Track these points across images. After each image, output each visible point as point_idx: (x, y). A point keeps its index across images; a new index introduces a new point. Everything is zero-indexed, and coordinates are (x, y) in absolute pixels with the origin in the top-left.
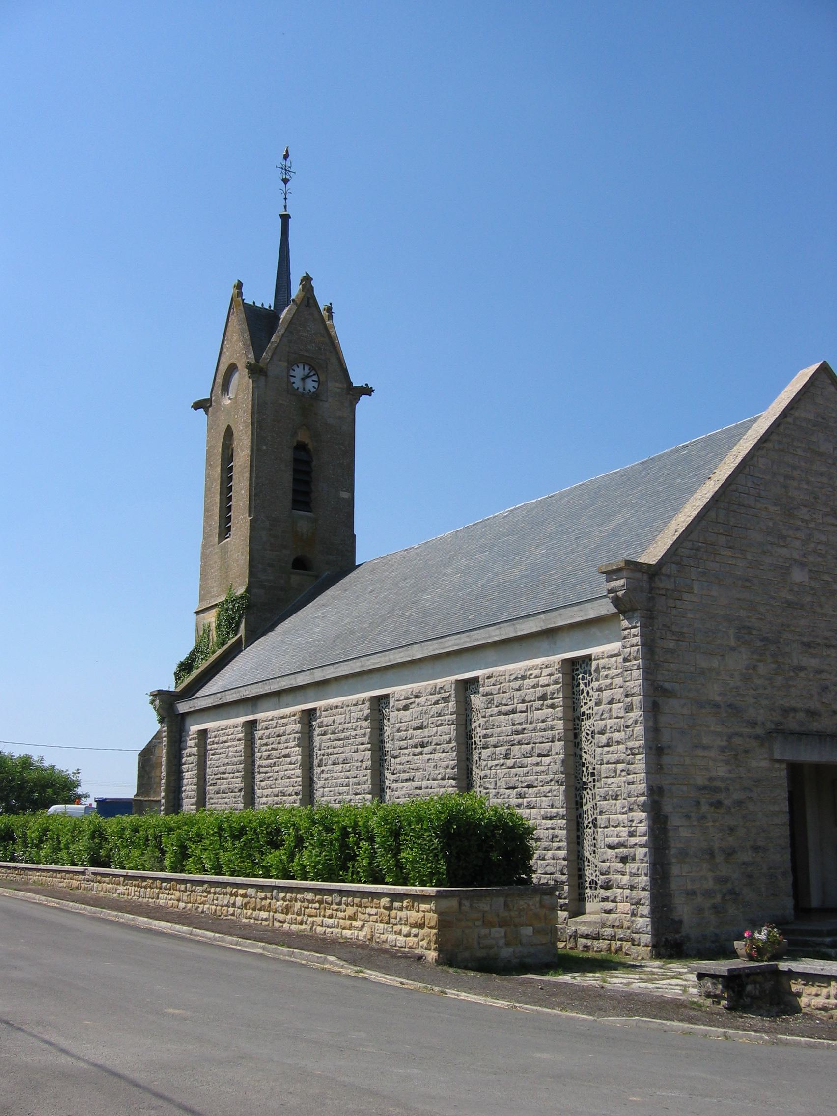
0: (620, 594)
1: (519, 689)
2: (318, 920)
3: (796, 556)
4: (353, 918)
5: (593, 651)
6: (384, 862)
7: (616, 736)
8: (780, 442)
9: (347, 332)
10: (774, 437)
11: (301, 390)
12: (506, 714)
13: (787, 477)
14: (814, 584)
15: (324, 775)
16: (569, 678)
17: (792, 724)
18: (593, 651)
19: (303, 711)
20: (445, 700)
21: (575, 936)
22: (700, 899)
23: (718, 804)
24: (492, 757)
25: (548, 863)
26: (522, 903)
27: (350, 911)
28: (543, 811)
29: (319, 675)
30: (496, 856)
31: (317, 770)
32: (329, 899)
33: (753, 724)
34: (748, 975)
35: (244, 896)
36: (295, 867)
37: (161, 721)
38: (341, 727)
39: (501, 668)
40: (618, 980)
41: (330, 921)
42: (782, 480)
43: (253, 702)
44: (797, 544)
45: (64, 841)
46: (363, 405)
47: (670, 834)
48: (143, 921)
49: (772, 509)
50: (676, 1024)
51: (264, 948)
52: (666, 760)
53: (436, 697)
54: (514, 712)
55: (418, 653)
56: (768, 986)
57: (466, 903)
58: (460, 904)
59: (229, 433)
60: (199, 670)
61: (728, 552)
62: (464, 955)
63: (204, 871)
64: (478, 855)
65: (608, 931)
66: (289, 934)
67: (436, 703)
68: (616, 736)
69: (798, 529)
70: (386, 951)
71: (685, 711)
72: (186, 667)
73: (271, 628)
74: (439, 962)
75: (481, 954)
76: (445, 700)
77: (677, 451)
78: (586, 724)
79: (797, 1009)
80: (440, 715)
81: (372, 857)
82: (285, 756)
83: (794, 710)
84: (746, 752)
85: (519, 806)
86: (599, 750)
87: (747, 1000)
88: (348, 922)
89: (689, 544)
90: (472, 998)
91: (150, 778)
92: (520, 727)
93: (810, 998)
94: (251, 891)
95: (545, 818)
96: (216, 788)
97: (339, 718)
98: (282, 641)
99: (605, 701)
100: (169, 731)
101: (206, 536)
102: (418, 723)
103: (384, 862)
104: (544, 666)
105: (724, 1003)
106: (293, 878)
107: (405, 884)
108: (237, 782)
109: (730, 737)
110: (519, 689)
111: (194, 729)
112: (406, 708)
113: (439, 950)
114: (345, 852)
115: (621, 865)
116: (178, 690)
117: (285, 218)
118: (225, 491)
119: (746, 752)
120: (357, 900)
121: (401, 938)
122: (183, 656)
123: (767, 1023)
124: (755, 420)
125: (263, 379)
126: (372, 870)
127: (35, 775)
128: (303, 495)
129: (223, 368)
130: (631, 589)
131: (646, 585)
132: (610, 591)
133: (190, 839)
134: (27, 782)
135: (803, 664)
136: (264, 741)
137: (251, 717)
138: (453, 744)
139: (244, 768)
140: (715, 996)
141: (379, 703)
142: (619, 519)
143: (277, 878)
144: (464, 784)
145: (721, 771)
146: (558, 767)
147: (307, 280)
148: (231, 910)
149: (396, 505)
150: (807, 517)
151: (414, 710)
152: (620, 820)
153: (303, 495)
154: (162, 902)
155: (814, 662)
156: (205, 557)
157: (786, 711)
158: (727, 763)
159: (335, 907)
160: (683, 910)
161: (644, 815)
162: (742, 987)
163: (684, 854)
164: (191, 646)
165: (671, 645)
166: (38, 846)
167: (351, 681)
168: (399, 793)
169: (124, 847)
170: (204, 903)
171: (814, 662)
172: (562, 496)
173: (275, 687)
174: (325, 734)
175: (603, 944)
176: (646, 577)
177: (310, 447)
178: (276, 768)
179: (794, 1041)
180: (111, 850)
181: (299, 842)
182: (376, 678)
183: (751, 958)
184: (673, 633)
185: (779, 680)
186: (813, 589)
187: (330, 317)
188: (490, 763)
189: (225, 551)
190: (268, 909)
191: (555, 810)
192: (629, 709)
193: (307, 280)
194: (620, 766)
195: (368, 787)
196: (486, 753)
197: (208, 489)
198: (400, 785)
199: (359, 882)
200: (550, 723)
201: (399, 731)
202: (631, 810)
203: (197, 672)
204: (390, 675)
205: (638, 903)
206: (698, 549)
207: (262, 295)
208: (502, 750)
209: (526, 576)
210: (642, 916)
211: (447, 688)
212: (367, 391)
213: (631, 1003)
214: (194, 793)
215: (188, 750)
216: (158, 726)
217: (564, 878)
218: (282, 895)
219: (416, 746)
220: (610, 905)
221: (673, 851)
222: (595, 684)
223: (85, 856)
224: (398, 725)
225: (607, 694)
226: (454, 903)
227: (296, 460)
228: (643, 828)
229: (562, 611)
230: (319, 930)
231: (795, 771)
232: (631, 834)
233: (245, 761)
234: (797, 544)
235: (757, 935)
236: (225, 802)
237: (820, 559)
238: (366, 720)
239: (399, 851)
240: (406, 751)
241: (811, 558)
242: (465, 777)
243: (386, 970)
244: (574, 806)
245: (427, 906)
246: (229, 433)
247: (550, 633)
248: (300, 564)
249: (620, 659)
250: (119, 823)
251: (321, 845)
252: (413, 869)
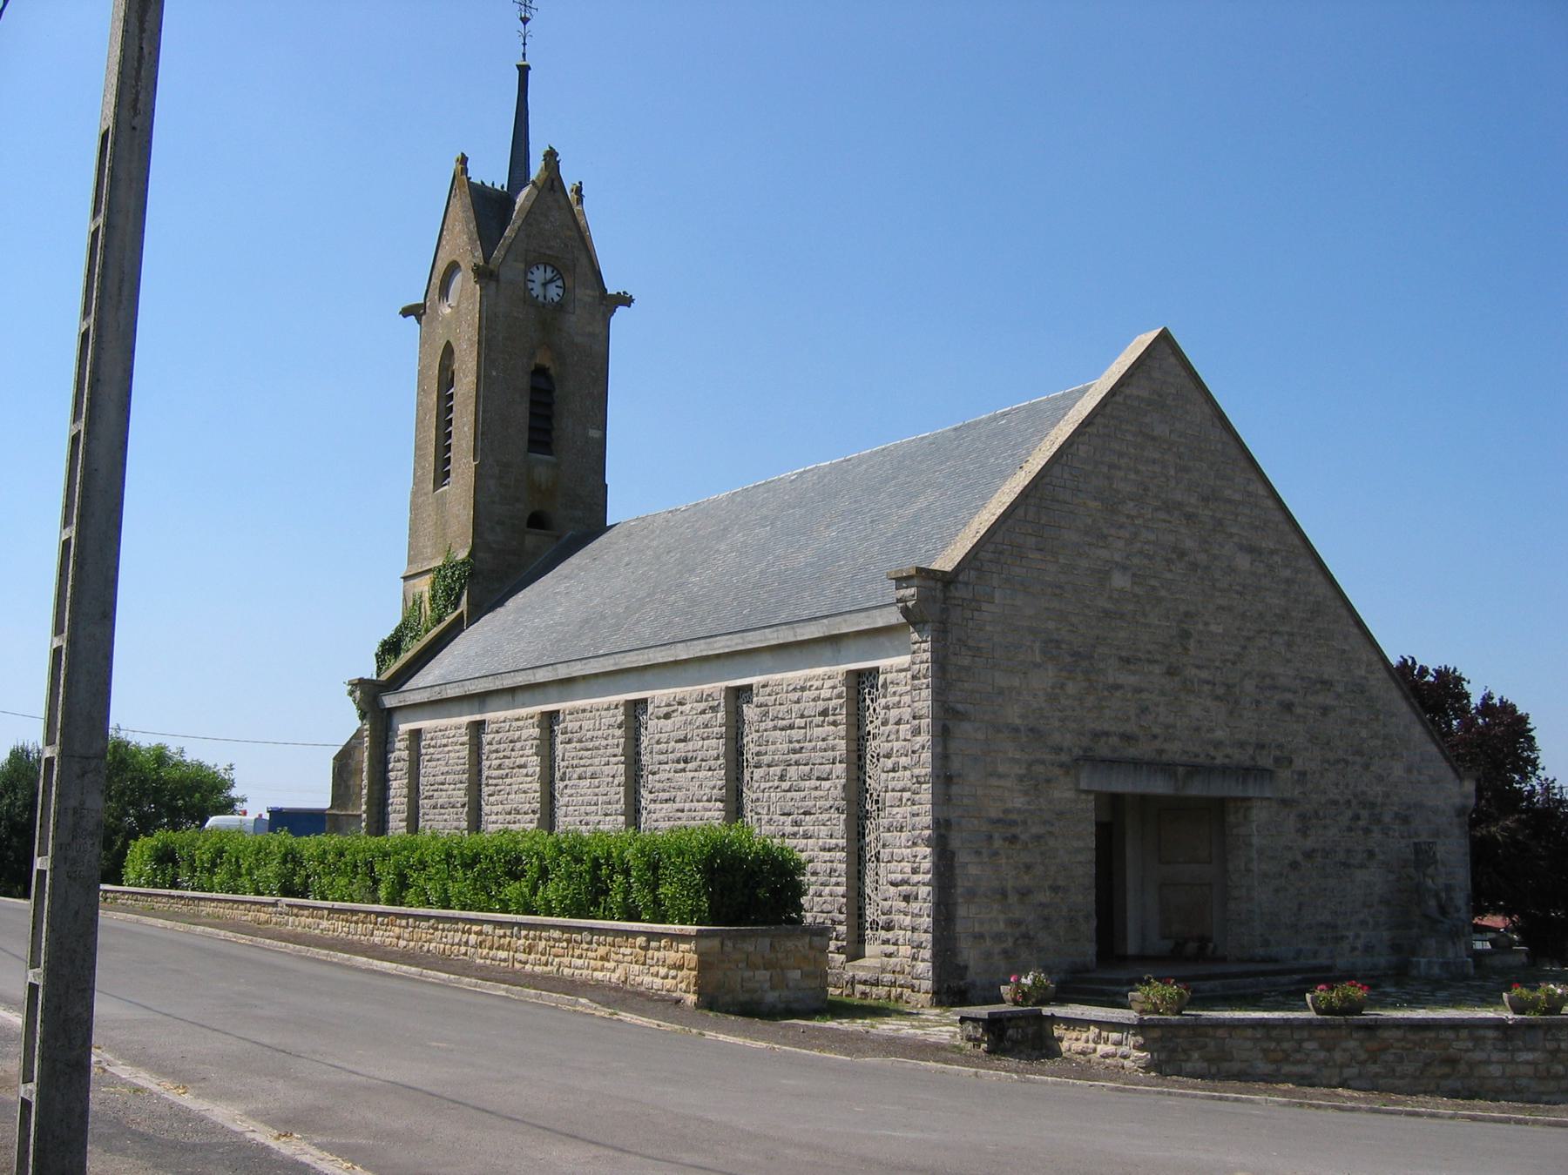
0: (910, 604)
1: (798, 702)
2: (566, 960)
3: (1117, 558)
4: (605, 958)
5: (882, 663)
6: (640, 897)
7: (903, 761)
8: (1105, 426)
9: (599, 219)
10: (1099, 420)
11: (541, 299)
12: (782, 729)
13: (1112, 466)
14: (1137, 590)
15: (568, 791)
16: (854, 692)
17: (1103, 750)
18: (882, 663)
19: (543, 713)
20: (714, 709)
21: (852, 982)
22: (989, 943)
23: (1013, 839)
24: (766, 778)
25: (822, 900)
26: (790, 944)
27: (602, 950)
28: (821, 842)
29: (563, 672)
30: (763, 893)
31: (559, 785)
32: (579, 938)
33: (1058, 750)
34: (1009, 1019)
35: (479, 933)
36: (538, 900)
37: (362, 717)
38: (589, 735)
39: (778, 676)
40: (887, 1027)
41: (580, 962)
42: (1105, 469)
43: (481, 699)
44: (1121, 544)
45: (245, 866)
46: (620, 319)
47: (958, 871)
48: (361, 960)
49: (1092, 504)
50: (931, 1064)
51: (507, 991)
52: (955, 790)
53: (703, 705)
54: (791, 727)
55: (682, 653)
56: (1030, 1031)
57: (729, 944)
58: (722, 944)
59: (448, 351)
60: (410, 654)
61: (1038, 556)
62: (721, 998)
63: (428, 903)
64: (744, 893)
65: (888, 977)
66: (533, 976)
67: (703, 712)
68: (903, 761)
69: (1121, 527)
70: (641, 994)
71: (981, 736)
72: (391, 648)
73: (500, 602)
74: (697, 1005)
75: (743, 997)
76: (714, 709)
77: (995, 419)
78: (872, 745)
79: (1059, 1054)
80: (706, 726)
81: (627, 892)
82: (520, 767)
83: (1107, 734)
84: (1048, 781)
85: (794, 835)
86: (884, 775)
87: (1008, 1044)
88: (600, 963)
89: (991, 547)
90: (731, 1039)
91: (347, 787)
92: (797, 746)
93: (1071, 1042)
94: (487, 928)
95: (823, 849)
96: (432, 802)
97: (587, 725)
98: (515, 621)
99: (892, 721)
100: (372, 730)
101: (417, 481)
102: (681, 734)
103: (640, 897)
104: (825, 678)
105: (984, 1046)
106: (535, 913)
107: (663, 922)
108: (460, 796)
109: (1030, 765)
110: (798, 702)
111: (404, 728)
112: (667, 716)
113: (699, 993)
114: (597, 885)
115: (904, 904)
116: (384, 677)
117: (524, 71)
118: (443, 426)
119: (1048, 781)
120: (610, 939)
121: (658, 981)
122: (387, 633)
123: (1023, 1064)
124: (1086, 390)
125: (493, 285)
126: (627, 906)
127: (176, 774)
128: (541, 435)
129: (442, 266)
130: (921, 600)
131: (939, 595)
132: (899, 601)
133: (411, 867)
134: (165, 783)
135: (1119, 682)
136: (494, 747)
137: (478, 717)
138: (722, 761)
139: (469, 779)
140: (976, 1039)
141: (636, 709)
142: (921, 502)
143: (517, 913)
144: (733, 808)
145: (1019, 802)
146: (838, 792)
147: (551, 156)
148: (463, 949)
149: (658, 451)
150: (1133, 513)
151: (677, 719)
152: (904, 857)
153: (541, 435)
154: (377, 940)
155: (1132, 680)
156: (415, 508)
157: (1097, 735)
158: (1026, 793)
159: (585, 946)
160: (969, 954)
161: (928, 850)
162: (1003, 1030)
163: (971, 894)
164: (397, 620)
165: (966, 662)
166: (209, 870)
167: (601, 680)
168: (659, 819)
169: (326, 874)
170: (430, 941)
171: (1132, 680)
172: (861, 461)
173: (508, 682)
174: (569, 742)
175: (882, 991)
176: (939, 585)
177: (552, 371)
178: (508, 781)
179: (1043, 1079)
180: (308, 876)
181: (544, 873)
182: (632, 678)
183: (1016, 1003)
184: (969, 648)
185: (1090, 700)
186: (1135, 595)
187: (580, 200)
188: (763, 785)
189: (441, 503)
190: (508, 948)
191: (834, 841)
192: (916, 732)
193: (551, 156)
194: (906, 795)
195: (621, 806)
196: (758, 773)
197: (420, 422)
198: (659, 806)
199: (612, 918)
200: (831, 742)
201: (658, 742)
202: (915, 844)
203: (404, 654)
204: (649, 676)
205: (919, 946)
206: (1001, 553)
207: (493, 172)
208: (777, 770)
209: (811, 565)
210: (923, 960)
211: (716, 695)
212: (625, 300)
213: (894, 1046)
214: (404, 807)
215: (397, 754)
216: (358, 723)
217: (842, 917)
218: (524, 933)
219: (678, 762)
220: (890, 948)
221: (960, 890)
222: (882, 701)
223: (275, 885)
224: (657, 736)
225: (894, 713)
226: (716, 943)
227: (534, 389)
228: (927, 865)
229: (847, 616)
230: (567, 971)
231: (1114, 803)
232: (915, 871)
233: (469, 770)
234: (1121, 544)
235: (1023, 980)
236: (444, 821)
237: (1146, 562)
238: (620, 727)
239: (657, 886)
240: (667, 767)
241: (1136, 561)
242: (734, 805)
243: (641, 1012)
244: (855, 835)
245: (687, 947)
246: (448, 351)
247: (834, 640)
248: (537, 521)
249: (909, 674)
250: (319, 845)
251: (570, 876)
252: (673, 906)
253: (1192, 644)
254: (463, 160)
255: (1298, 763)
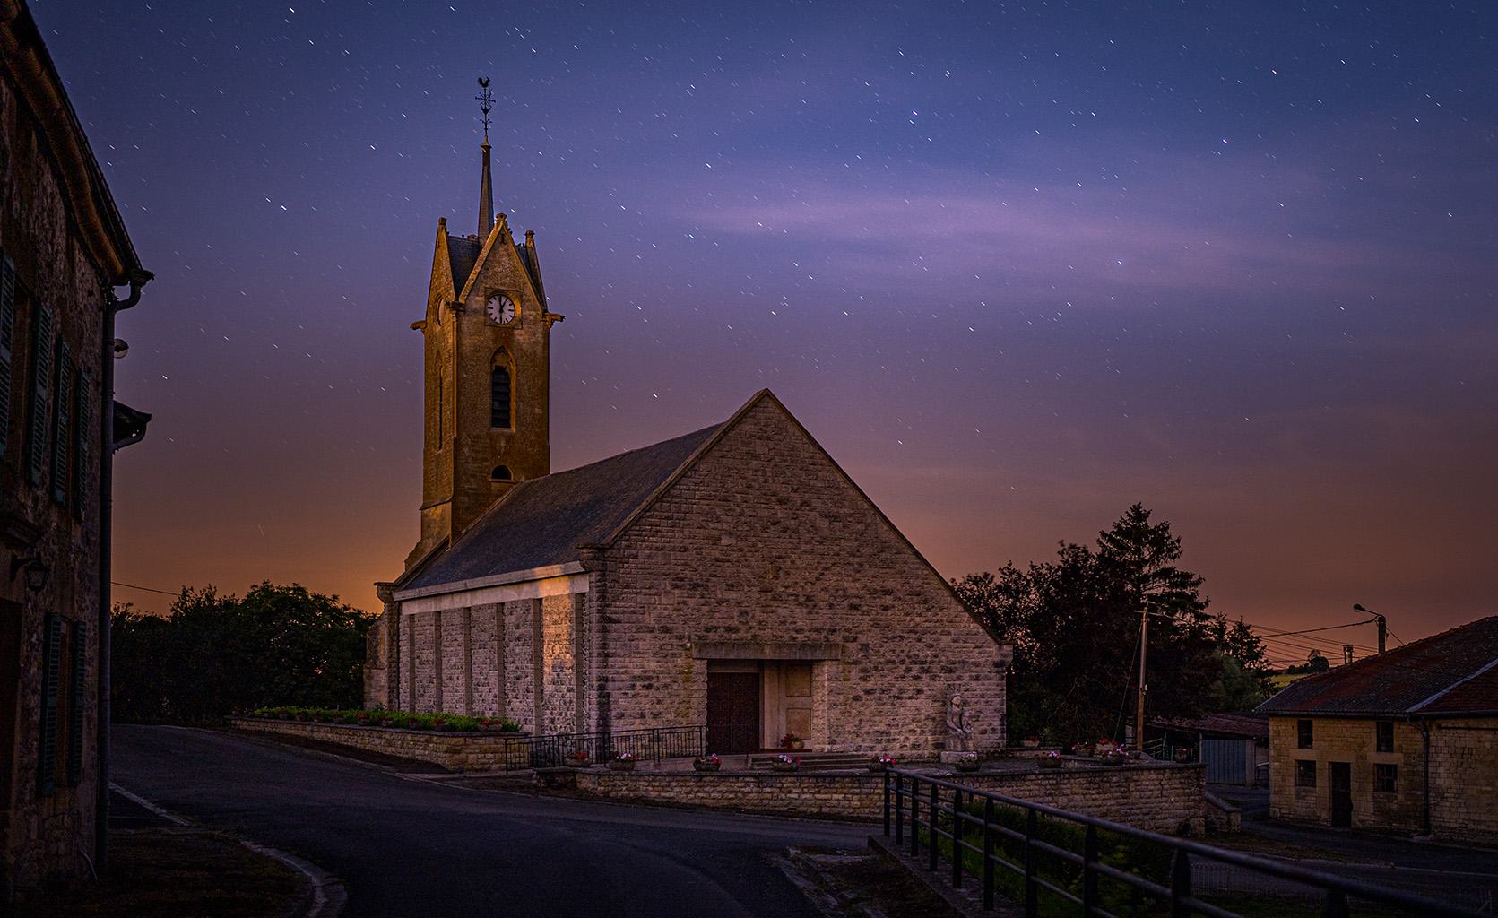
207: (466, 226)
227: (494, 384)
253: (781, 574)
254: (443, 221)
255: (863, 639)
